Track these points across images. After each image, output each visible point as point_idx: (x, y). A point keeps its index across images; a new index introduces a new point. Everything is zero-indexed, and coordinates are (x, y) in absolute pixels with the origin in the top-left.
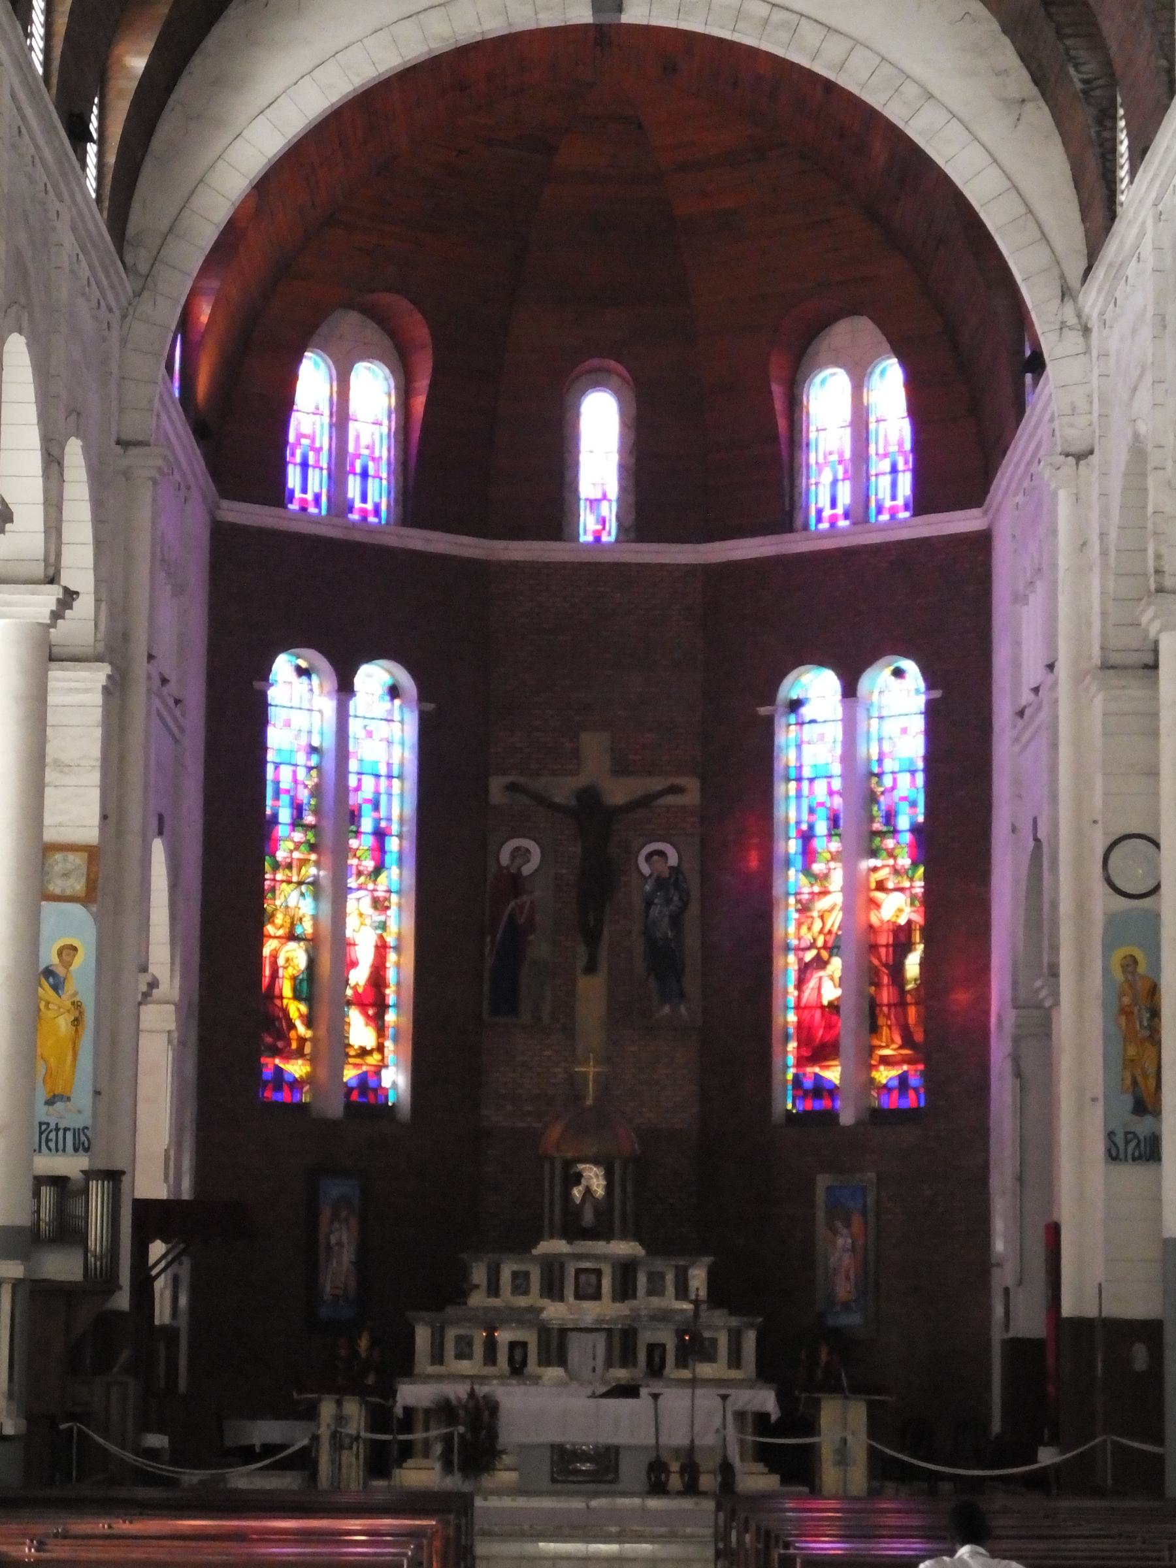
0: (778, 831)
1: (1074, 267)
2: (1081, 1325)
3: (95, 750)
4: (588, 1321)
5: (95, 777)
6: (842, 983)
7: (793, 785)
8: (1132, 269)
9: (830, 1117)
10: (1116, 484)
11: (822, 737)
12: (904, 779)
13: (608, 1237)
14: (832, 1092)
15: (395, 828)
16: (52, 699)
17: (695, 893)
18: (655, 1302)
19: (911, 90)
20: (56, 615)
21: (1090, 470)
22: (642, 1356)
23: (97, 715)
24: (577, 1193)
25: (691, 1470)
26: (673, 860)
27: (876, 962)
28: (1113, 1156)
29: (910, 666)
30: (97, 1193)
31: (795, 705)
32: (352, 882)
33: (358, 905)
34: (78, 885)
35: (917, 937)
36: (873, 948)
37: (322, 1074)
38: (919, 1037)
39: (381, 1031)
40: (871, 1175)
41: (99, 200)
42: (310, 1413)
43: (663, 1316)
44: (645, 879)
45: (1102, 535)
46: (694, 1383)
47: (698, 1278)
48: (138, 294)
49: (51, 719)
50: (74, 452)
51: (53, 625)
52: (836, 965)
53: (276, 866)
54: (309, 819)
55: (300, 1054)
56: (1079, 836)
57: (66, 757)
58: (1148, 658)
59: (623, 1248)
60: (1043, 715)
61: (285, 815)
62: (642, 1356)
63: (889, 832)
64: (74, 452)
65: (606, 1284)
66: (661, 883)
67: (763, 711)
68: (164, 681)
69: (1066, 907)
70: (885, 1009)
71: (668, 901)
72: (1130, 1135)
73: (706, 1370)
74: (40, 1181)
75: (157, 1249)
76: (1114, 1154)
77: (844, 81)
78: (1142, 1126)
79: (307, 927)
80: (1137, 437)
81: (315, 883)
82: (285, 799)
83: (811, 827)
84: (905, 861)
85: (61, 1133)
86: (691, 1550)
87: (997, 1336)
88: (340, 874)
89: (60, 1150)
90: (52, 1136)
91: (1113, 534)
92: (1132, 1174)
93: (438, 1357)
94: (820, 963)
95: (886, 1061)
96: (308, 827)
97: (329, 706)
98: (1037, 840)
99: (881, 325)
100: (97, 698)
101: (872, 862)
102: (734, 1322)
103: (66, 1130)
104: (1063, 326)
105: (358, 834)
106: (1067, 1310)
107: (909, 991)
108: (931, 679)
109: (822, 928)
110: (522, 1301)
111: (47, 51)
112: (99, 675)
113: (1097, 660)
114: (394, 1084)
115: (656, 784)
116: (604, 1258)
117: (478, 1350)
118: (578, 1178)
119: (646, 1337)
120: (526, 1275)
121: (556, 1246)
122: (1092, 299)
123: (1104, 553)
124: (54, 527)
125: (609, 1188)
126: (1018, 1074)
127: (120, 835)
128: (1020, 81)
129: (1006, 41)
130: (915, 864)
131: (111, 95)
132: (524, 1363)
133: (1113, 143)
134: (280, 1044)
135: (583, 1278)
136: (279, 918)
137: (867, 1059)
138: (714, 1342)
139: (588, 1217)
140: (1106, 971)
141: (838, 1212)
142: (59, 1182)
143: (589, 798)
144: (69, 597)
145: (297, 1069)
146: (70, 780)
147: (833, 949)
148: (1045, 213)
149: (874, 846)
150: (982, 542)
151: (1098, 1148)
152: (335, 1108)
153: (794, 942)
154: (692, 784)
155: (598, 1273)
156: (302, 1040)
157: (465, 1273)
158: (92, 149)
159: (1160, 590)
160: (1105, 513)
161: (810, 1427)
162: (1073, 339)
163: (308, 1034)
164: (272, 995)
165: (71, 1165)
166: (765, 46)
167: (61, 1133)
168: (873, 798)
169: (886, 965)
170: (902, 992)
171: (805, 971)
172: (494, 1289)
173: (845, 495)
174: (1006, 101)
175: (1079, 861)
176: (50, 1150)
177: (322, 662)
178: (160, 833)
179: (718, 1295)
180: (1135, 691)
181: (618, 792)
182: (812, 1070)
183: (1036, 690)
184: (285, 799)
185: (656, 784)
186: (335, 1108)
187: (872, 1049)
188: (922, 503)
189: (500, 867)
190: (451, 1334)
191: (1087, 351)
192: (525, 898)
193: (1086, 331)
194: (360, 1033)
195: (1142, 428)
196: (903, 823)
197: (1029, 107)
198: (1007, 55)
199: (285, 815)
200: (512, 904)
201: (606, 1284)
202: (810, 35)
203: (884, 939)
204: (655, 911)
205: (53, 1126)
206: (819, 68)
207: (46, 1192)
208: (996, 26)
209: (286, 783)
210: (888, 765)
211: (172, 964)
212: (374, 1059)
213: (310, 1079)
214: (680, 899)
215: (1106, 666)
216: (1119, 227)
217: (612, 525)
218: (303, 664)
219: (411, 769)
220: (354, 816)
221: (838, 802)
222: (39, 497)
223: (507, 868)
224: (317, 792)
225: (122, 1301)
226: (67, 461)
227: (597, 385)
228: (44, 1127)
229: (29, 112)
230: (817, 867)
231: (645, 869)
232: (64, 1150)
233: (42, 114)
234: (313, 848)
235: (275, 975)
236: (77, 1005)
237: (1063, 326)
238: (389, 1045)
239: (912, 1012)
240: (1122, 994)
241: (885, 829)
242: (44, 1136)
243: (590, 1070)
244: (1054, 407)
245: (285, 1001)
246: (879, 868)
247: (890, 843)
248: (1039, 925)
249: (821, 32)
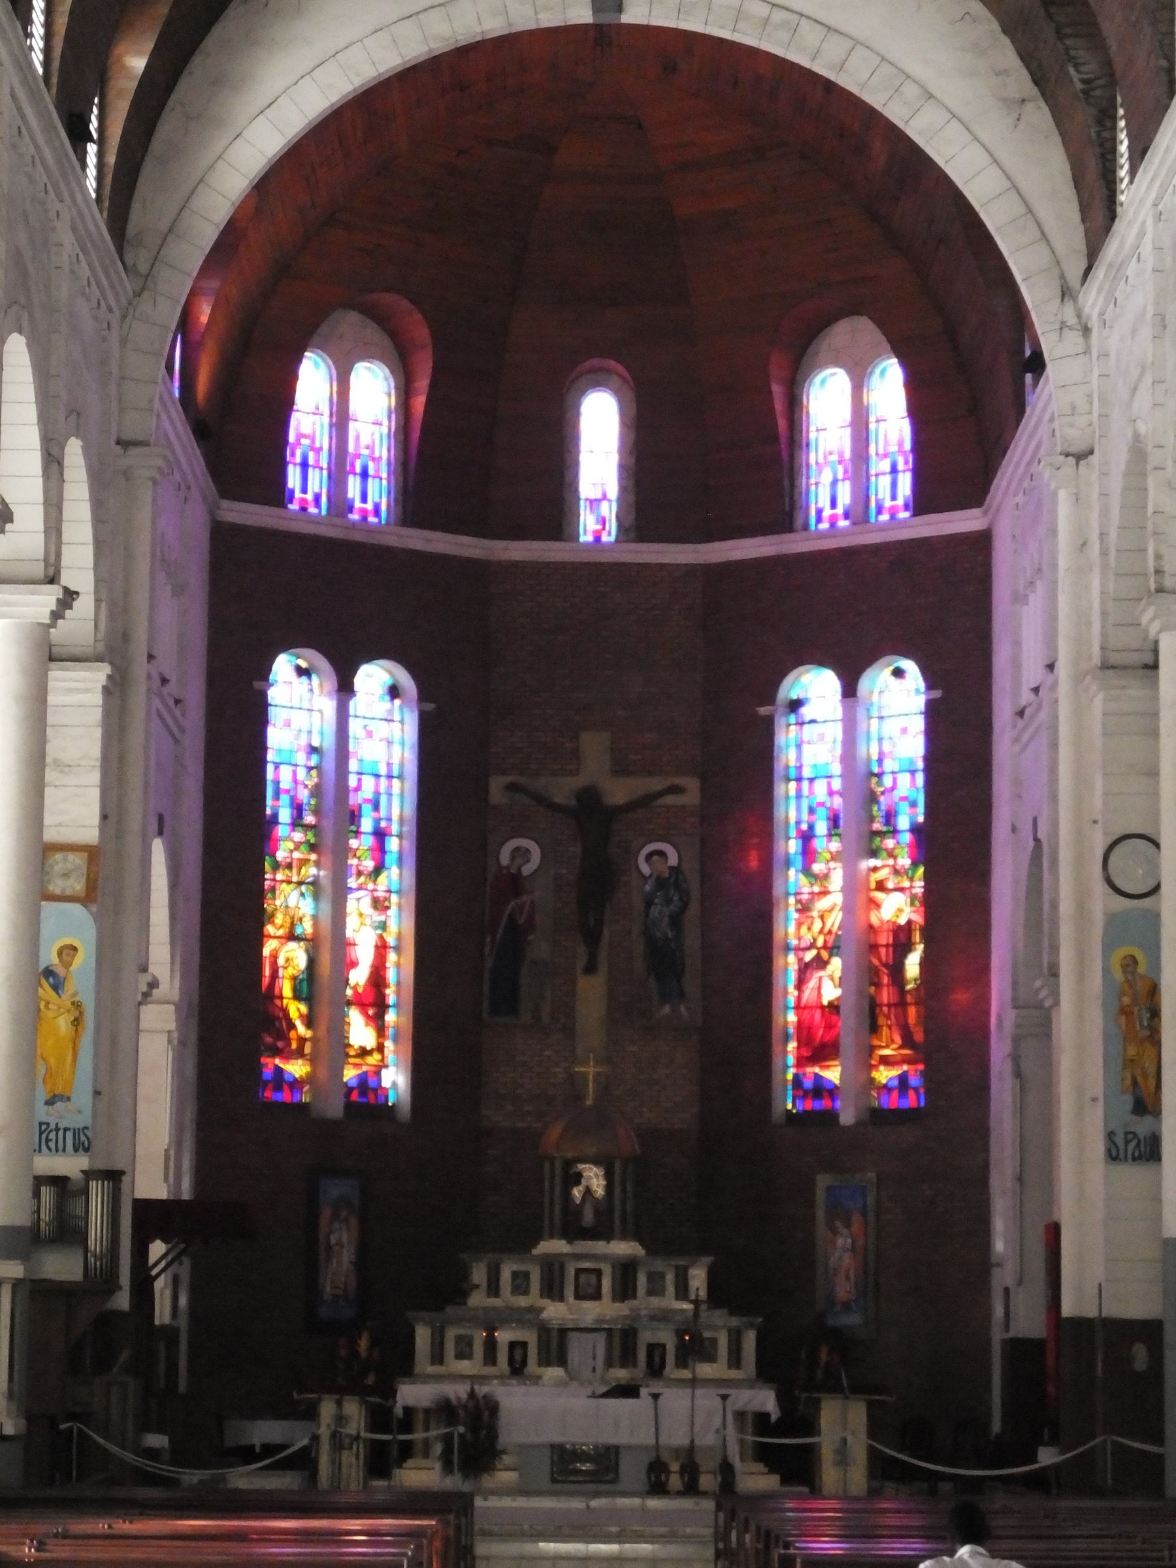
0: (778, 831)
1: (1074, 267)
2: (1081, 1325)
3: (95, 750)
4: (588, 1321)
5: (95, 777)
6: (842, 983)
7: (793, 785)
8: (1132, 269)
9: (830, 1117)
10: (1116, 484)
13: (608, 1237)
16: (52, 699)
17: (695, 893)
18: (655, 1302)
19: (911, 90)
20: (56, 615)
21: (1090, 470)
22: (642, 1356)
23: (97, 715)
24: (577, 1193)
25: (691, 1470)
26: (673, 860)
27: (876, 962)
28: (1113, 1156)
29: (910, 666)
30: (97, 1193)
31: (795, 705)
32: (352, 882)
33: (358, 905)
34: (78, 885)
35: (917, 937)
36: (873, 948)
37: (322, 1074)
38: (919, 1037)
39: (381, 1031)
40: (871, 1175)
41: (99, 200)
43: (663, 1316)
44: (645, 879)
46: (694, 1383)
47: (698, 1278)
48: (138, 294)
49: (51, 719)
50: (74, 452)
51: (53, 625)
53: (276, 866)
55: (300, 1054)
56: (1079, 836)
57: (66, 757)
58: (1148, 658)
60: (1043, 715)
61: (285, 815)
62: (642, 1356)
63: (889, 832)
64: (74, 452)
65: (606, 1284)
66: (661, 883)
67: (763, 711)
68: (164, 681)
69: (1066, 907)
70: (885, 1009)
71: (668, 901)
72: (1130, 1135)
73: (706, 1370)
74: (40, 1181)
75: (157, 1249)
76: (1114, 1154)
77: (844, 81)
78: (1142, 1126)
79: (307, 927)
80: (1137, 437)
81: (315, 883)
82: (285, 799)
83: (811, 827)
85: (61, 1133)
87: (997, 1336)
88: (340, 874)
89: (60, 1150)
90: (52, 1136)
91: (1113, 534)
92: (1132, 1174)
93: (438, 1357)
94: (820, 963)
95: (886, 1061)
96: (308, 827)
97: (329, 706)
98: (1037, 840)
99: (881, 325)
100: (97, 698)
102: (734, 1322)
103: (66, 1130)
104: (1063, 326)
106: (1067, 1310)
107: (909, 991)
108: (931, 679)
109: (822, 928)
110: (522, 1301)
112: (99, 675)
113: (1097, 660)
114: (394, 1084)
115: (656, 784)
116: (604, 1258)
117: (478, 1350)
118: (578, 1178)
119: (646, 1337)
120: (526, 1275)
121: (556, 1246)
122: (1092, 299)
123: (1104, 553)
124: (54, 527)
125: (609, 1188)
127: (120, 835)
128: (1020, 81)
129: (1006, 41)
132: (524, 1363)
133: (1113, 143)
134: (280, 1044)
135: (583, 1278)
136: (279, 918)
137: (867, 1059)
138: (714, 1342)
139: (588, 1217)
140: (1106, 971)
141: (838, 1212)
142: (59, 1182)
144: (69, 597)
145: (297, 1069)
146: (70, 780)
147: (833, 949)
148: (1045, 213)
149: (874, 846)
150: (982, 542)
151: (1098, 1148)
152: (335, 1108)
154: (692, 784)
155: (598, 1273)
156: (302, 1040)
157: (465, 1273)
160: (1105, 513)
162: (1073, 339)
163: (308, 1034)
164: (272, 995)
165: (71, 1165)
166: (765, 46)
167: (61, 1133)
169: (886, 965)
170: (902, 992)
171: (805, 971)
172: (494, 1289)
174: (1006, 101)
175: (1079, 861)
176: (50, 1150)
177: (322, 662)
178: (160, 833)
179: (718, 1295)
180: (1135, 691)
181: (618, 792)
182: (812, 1070)
183: (1036, 690)
184: (285, 799)
185: (656, 784)
186: (335, 1108)
187: (872, 1049)
188: (922, 503)
189: (500, 867)
190: (451, 1334)
191: (1087, 351)
192: (525, 898)
193: (1086, 331)
195: (1142, 428)
196: (903, 823)
197: (1029, 107)
198: (1007, 55)
199: (285, 815)
200: (512, 904)
201: (606, 1284)
202: (810, 35)
203: (884, 939)
204: (655, 911)
205: (53, 1126)
206: (819, 68)
207: (46, 1192)
208: (996, 26)
209: (286, 783)
210: (888, 765)
211: (172, 964)
212: (374, 1059)
213: (310, 1079)
214: (680, 899)
215: (1106, 666)
216: (1119, 227)
217: (612, 525)
218: (303, 664)
219: (411, 769)
220: (354, 816)
221: (838, 802)
222: (39, 497)
223: (507, 868)
225: (122, 1301)
226: (67, 461)
227: (597, 385)
228: (44, 1127)
229: (29, 112)
230: (817, 867)
231: (645, 869)
232: (64, 1150)
233: (42, 114)
234: (313, 848)
235: (275, 975)
236: (77, 1005)
237: (1063, 326)
238: (389, 1045)
239: (912, 1012)
240: (1122, 994)
241: (885, 829)
242: (44, 1136)
243: (590, 1070)
244: (1054, 407)
245: (285, 1001)
246: (879, 868)
247: (890, 843)
248: (1039, 925)
249: (821, 32)
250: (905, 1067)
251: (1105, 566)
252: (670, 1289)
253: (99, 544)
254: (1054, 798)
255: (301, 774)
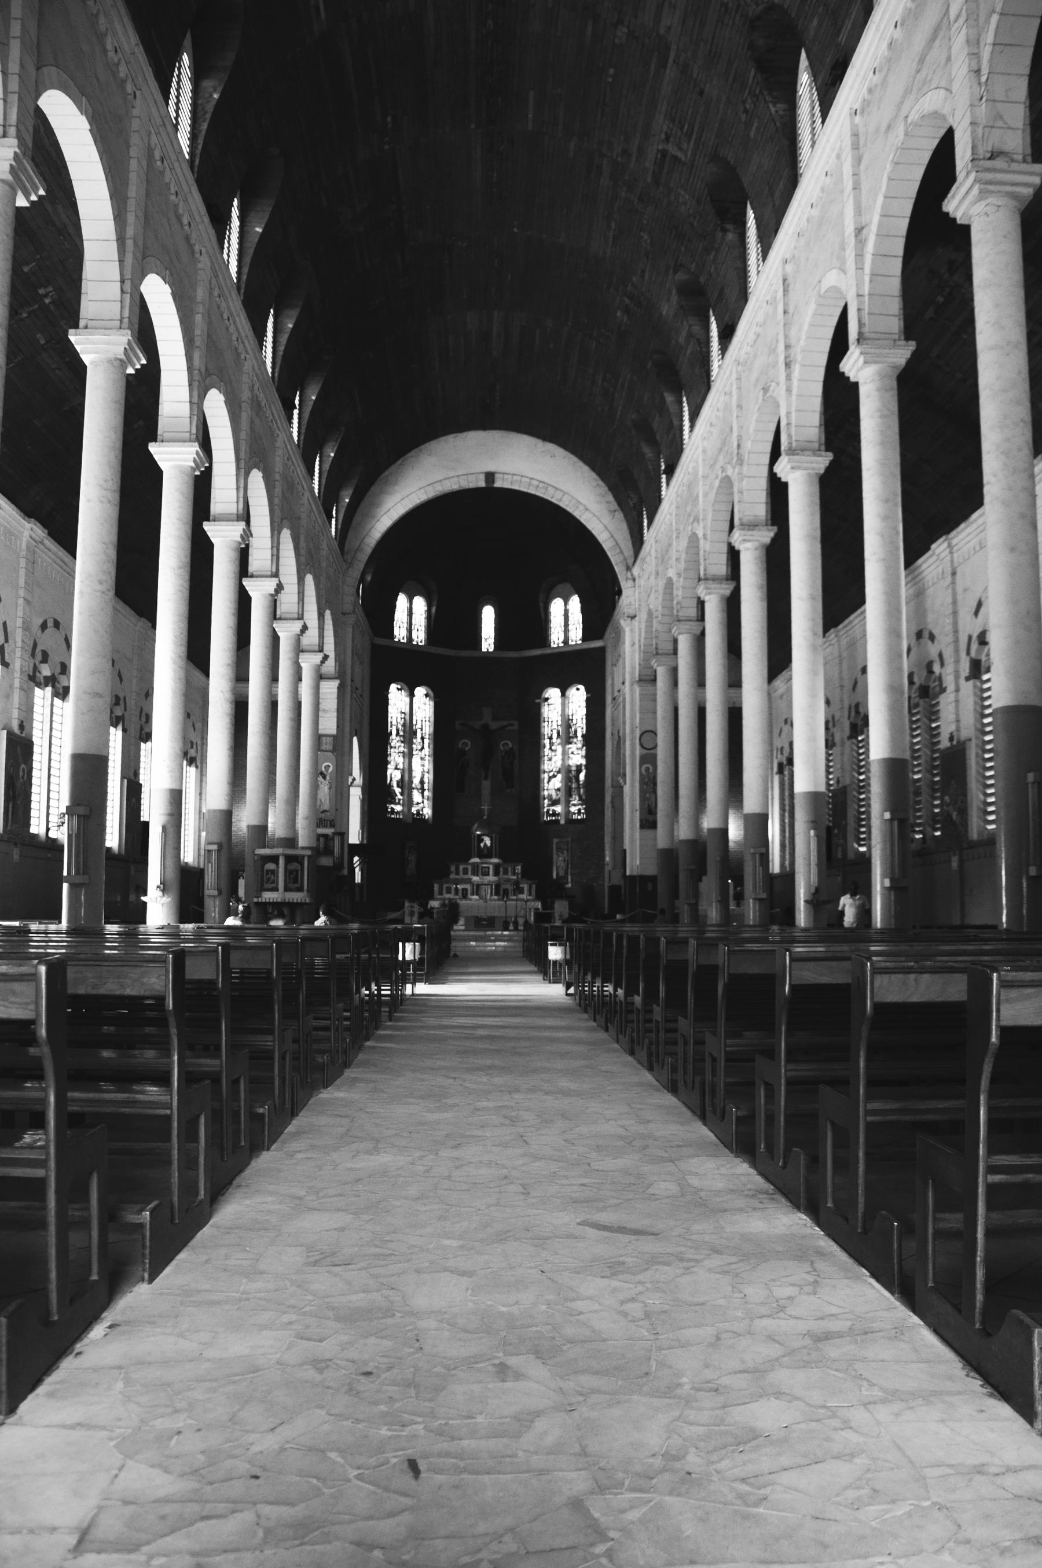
0: (542, 737)
1: (630, 561)
2: (632, 878)
3: (335, 707)
4: (486, 882)
5: (335, 714)
6: (561, 782)
7: (546, 723)
8: (648, 559)
9: (557, 821)
10: (643, 625)
11: (555, 709)
12: (579, 721)
13: (491, 857)
14: (558, 815)
15: (427, 736)
16: (321, 691)
18: (506, 877)
19: (581, 507)
20: (322, 662)
21: (636, 622)
22: (502, 892)
23: (335, 695)
24: (482, 845)
25: (516, 923)
26: (510, 746)
28: (642, 827)
29: (582, 687)
30: (337, 840)
31: (547, 699)
32: (414, 753)
33: (416, 761)
34: (330, 748)
35: (583, 768)
36: (570, 771)
37: (406, 810)
38: (584, 797)
39: (423, 797)
40: (570, 839)
41: (336, 538)
42: (403, 907)
43: (509, 880)
45: (639, 641)
46: (517, 900)
47: (519, 868)
48: (348, 569)
49: (321, 696)
50: (328, 614)
51: (321, 665)
52: (559, 776)
53: (391, 747)
54: (401, 733)
55: (399, 803)
56: (633, 731)
57: (326, 708)
58: (653, 678)
59: (495, 860)
60: (621, 699)
61: (394, 732)
62: (502, 892)
64: (328, 614)
65: (491, 872)
67: (538, 701)
68: (357, 689)
69: (628, 753)
72: (647, 821)
73: (521, 896)
74: (319, 836)
75: (356, 859)
77: (561, 504)
78: (650, 818)
79: (401, 766)
80: (650, 609)
81: (403, 752)
84: (580, 745)
86: (517, 944)
87: (607, 884)
88: (411, 750)
89: (325, 827)
91: (642, 640)
92: (649, 833)
93: (441, 893)
94: (554, 776)
95: (574, 805)
96: (401, 736)
97: (408, 700)
98: (619, 737)
99: (573, 586)
100: (336, 691)
101: (570, 746)
102: (529, 882)
104: (627, 578)
105: (416, 738)
106: (628, 873)
108: (587, 691)
110: (466, 877)
111: (319, 489)
112: (336, 683)
113: (637, 679)
115: (505, 723)
116: (491, 863)
117: (453, 891)
118: (482, 840)
119: (503, 887)
120: (467, 869)
121: (476, 860)
122: (636, 570)
123: (640, 646)
124: (321, 636)
125: (491, 844)
126: (613, 806)
127: (343, 731)
128: (614, 506)
129: (610, 493)
130: (583, 746)
131: (340, 506)
132: (467, 894)
133: (642, 522)
136: (392, 763)
137: (568, 804)
138: (523, 888)
139: (485, 852)
140: (640, 771)
141: (560, 849)
142: (325, 836)
143: (486, 727)
144: (326, 658)
145: (398, 808)
146: (328, 715)
147: (559, 772)
148: (623, 546)
150: (602, 650)
151: (638, 825)
152: (410, 821)
153: (547, 770)
154: (516, 723)
155: (489, 868)
156: (399, 800)
157: (449, 868)
158: (296, 412)
159: (657, 654)
160: (640, 635)
161: (552, 908)
162: (630, 583)
163: (401, 797)
164: (390, 786)
165: (329, 831)
166: (538, 494)
168: (570, 727)
171: (550, 778)
172: (457, 873)
173: (562, 638)
174: (610, 511)
175: (633, 740)
177: (406, 687)
178: (356, 735)
179: (525, 874)
180: (650, 688)
181: (494, 725)
182: (552, 808)
183: (619, 691)
185: (505, 723)
186: (410, 821)
187: (570, 801)
188: (585, 638)
190: (445, 886)
191: (634, 586)
193: (634, 580)
194: (417, 796)
195: (651, 607)
196: (579, 734)
197: (616, 513)
198: (610, 498)
199: (394, 732)
201: (491, 872)
202: (551, 491)
203: (574, 768)
206: (554, 500)
207: (322, 839)
208: (606, 488)
209: (394, 723)
210: (575, 718)
211: (272, 560)
212: (421, 805)
213: (402, 811)
215: (640, 680)
216: (645, 546)
217: (492, 646)
218: (399, 687)
219: (432, 719)
220: (415, 733)
221: (560, 729)
222: (317, 626)
224: (404, 725)
225: (345, 872)
226: (326, 617)
227: (487, 604)
229: (313, 506)
230: (553, 748)
231: (502, 748)
233: (318, 508)
234: (402, 742)
235: (391, 780)
237: (627, 578)
238: (426, 802)
239: (582, 791)
243: (486, 808)
244: (625, 603)
246: (573, 747)
247: (575, 740)
248: (619, 764)
249: (554, 490)
250: (580, 807)
251: (640, 650)
252: (510, 873)
253: (336, 644)
254: (624, 723)
255: (399, 720)
